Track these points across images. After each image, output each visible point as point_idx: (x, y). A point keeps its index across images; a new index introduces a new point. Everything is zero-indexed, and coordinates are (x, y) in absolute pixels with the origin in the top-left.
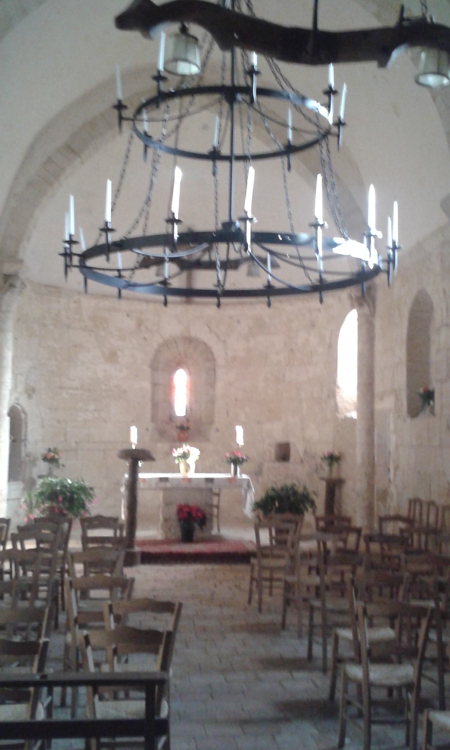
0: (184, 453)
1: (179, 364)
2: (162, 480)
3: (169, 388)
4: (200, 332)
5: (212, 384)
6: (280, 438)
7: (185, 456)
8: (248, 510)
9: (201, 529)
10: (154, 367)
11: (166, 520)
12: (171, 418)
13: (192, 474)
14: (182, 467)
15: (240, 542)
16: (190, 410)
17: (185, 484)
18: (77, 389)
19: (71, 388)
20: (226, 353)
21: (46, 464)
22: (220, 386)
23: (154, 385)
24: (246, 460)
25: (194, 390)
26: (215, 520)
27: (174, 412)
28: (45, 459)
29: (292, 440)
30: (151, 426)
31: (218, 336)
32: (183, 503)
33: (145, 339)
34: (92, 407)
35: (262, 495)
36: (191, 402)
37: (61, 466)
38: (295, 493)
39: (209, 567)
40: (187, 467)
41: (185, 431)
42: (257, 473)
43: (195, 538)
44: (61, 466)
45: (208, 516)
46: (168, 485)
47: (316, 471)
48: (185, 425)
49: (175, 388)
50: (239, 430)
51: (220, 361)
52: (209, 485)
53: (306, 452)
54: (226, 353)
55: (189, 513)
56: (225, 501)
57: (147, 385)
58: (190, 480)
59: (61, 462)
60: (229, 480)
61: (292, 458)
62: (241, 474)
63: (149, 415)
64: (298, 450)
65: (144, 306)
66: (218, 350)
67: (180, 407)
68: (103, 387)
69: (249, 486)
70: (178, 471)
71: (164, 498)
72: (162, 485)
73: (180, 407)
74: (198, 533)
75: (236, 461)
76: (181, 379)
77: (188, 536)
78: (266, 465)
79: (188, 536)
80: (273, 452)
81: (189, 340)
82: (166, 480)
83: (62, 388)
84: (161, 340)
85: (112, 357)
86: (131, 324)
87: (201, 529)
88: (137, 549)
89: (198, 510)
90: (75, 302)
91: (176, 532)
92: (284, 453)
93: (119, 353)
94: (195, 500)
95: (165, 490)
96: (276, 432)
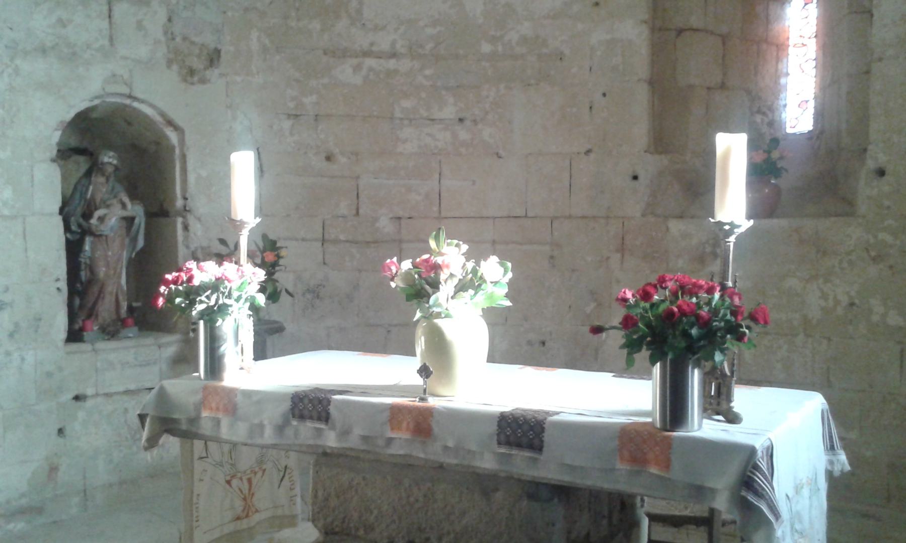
18: (394, 55)
19: (367, 54)
34: (449, 112)
50: (243, 165)
68: (486, 48)
72: (306, 430)
83: (340, 54)
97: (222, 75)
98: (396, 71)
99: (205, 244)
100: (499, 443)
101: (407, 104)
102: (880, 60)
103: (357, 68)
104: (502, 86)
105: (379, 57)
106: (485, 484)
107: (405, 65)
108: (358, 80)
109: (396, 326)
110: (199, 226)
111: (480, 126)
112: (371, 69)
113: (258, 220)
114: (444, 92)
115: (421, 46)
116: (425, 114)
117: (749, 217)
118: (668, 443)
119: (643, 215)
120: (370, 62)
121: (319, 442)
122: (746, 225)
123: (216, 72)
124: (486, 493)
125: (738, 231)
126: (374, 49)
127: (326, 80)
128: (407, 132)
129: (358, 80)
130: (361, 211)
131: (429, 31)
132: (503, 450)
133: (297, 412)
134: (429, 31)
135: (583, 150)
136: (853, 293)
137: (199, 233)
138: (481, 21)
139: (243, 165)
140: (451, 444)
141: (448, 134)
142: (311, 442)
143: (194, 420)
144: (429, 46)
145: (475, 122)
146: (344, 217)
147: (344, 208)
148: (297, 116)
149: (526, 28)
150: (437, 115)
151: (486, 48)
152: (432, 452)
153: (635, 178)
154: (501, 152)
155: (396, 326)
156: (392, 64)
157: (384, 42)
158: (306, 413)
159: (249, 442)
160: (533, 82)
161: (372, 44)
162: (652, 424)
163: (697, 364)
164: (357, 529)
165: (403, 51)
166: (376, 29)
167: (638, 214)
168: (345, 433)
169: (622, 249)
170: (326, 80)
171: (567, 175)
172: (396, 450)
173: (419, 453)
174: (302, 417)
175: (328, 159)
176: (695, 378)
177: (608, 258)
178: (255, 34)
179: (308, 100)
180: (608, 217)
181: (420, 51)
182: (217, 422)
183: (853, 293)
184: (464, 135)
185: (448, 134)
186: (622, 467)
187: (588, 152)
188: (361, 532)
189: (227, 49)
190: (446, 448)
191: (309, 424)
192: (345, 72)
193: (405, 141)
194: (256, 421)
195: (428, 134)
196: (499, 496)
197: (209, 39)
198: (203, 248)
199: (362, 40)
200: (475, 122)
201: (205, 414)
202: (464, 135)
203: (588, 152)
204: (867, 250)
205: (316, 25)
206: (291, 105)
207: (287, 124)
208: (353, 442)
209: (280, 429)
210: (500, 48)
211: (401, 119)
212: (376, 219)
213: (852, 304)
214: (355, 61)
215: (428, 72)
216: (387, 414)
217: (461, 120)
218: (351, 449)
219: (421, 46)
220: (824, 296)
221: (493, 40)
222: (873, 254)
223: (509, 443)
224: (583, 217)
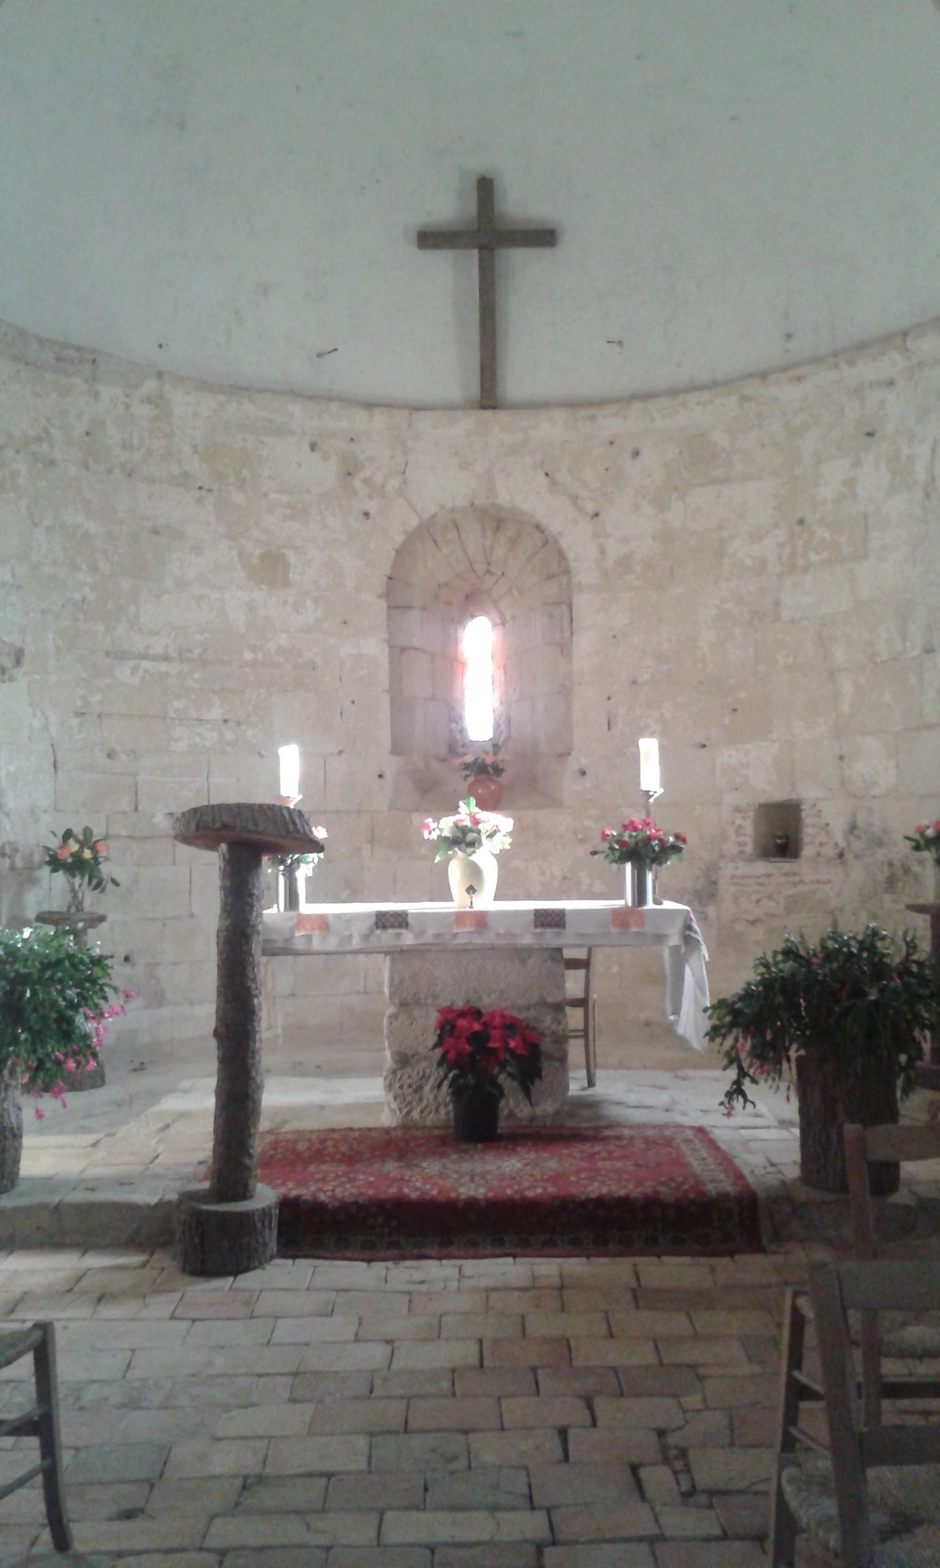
0: (464, 831)
1: (471, 601)
2: (383, 921)
3: (446, 664)
4: (524, 493)
5: (565, 648)
6: (769, 788)
7: (464, 839)
8: (691, 1020)
9: (528, 1094)
10: (396, 594)
11: (403, 1060)
12: (455, 745)
13: (486, 902)
14: (455, 873)
15: (661, 1140)
16: (505, 723)
17: (464, 935)
18: (166, 658)
19: (144, 656)
20: (603, 551)
21: (60, 876)
22: (585, 644)
23: (399, 652)
24: (675, 849)
25: (515, 665)
26: (575, 1050)
27: (462, 731)
28: (55, 863)
29: (807, 793)
30: (392, 766)
31: (574, 499)
32: (460, 1004)
33: (366, 514)
34: (215, 713)
35: (743, 976)
36: (506, 702)
37: (110, 886)
38: (879, 970)
39: (548, 1268)
40: (474, 872)
41: (490, 777)
42: (704, 894)
43: (503, 1125)
44: (110, 886)
45: (546, 1045)
46: (408, 939)
47: (891, 882)
48: (489, 760)
49: (463, 664)
50: (649, 748)
51: (585, 572)
52: (550, 937)
53: (853, 828)
54: (603, 551)
55: (479, 1040)
56: (608, 981)
57: (375, 648)
58: (481, 920)
59: (106, 869)
60: (620, 918)
61: (808, 851)
62: (657, 902)
63: (385, 737)
64: (825, 819)
65: (360, 418)
66: (577, 542)
67: (480, 716)
68: (248, 656)
69: (688, 939)
70: (447, 896)
71: (396, 986)
72: (387, 937)
73: (480, 716)
74: (514, 1107)
75: (641, 852)
76: (479, 640)
77: (477, 1124)
78: (728, 870)
79: (477, 1124)
80: (746, 832)
81: (496, 519)
82: (399, 920)
83: (118, 655)
84: (414, 522)
85: (271, 568)
86: (322, 472)
87: (528, 1094)
88: (264, 1195)
89: (511, 1026)
90: (149, 401)
91: (437, 1107)
92: (781, 834)
93: (291, 557)
94: (501, 991)
95: (398, 954)
96: (758, 771)
97: (26, 674)
98: (168, 674)
99: (12, 838)
100: (536, 926)
101: (178, 704)
102: (579, 684)
103: (134, 670)
104: (262, 691)
105: (154, 658)
106: (521, 954)
107: (174, 668)
108: (135, 681)
109: (171, 919)
110: (7, 821)
111: (243, 727)
112: (146, 671)
113: (301, 797)
114: (211, 695)
115: (190, 651)
116: (195, 715)
117: (662, 786)
118: (641, 915)
119: (389, 810)
120: (146, 664)
121: (398, 943)
122: (661, 791)
123: (22, 670)
124: (523, 961)
125: (656, 795)
126: (151, 652)
127: (108, 681)
128: (178, 732)
129: (135, 681)
130: (140, 808)
131: (198, 637)
132: (539, 930)
133: (380, 924)
134: (198, 637)
135: (336, 751)
136: (566, 870)
137: (8, 828)
138: (243, 630)
139: (649, 748)
140: (502, 931)
141: (215, 734)
142: (392, 944)
143: (289, 940)
144: (197, 651)
145: (239, 723)
146: (124, 813)
147: (125, 803)
148: (83, 714)
149: (283, 640)
150: (206, 716)
151: (248, 656)
152: (488, 938)
153: (380, 776)
154: (263, 752)
155: (171, 919)
156: (163, 667)
157: (158, 646)
158: (387, 924)
159: (340, 949)
160: (290, 688)
161: (148, 647)
162: (626, 906)
163: (651, 870)
164: (426, 999)
165: (174, 654)
166: (152, 633)
167: (385, 807)
168: (421, 933)
169: (372, 840)
170: (108, 681)
171: (322, 773)
172: (461, 940)
173: (478, 940)
174: (384, 927)
175: (109, 756)
176: (650, 877)
177: (360, 849)
178: (51, 635)
179: (95, 698)
180: (359, 812)
181: (189, 655)
182: (309, 938)
183: (566, 870)
184: (229, 735)
185: (215, 734)
186: (614, 930)
187: (340, 753)
188: (430, 1001)
189: (29, 650)
190: (498, 935)
191: (391, 931)
192: (124, 672)
193: (177, 740)
194: (347, 933)
195: (197, 734)
196: (531, 961)
197: (14, 639)
198: (10, 843)
199: (140, 645)
200: (239, 723)
201: (298, 934)
202: (229, 735)
203: (340, 753)
204: (575, 834)
205: (100, 628)
206: (79, 703)
207: (75, 722)
208: (428, 938)
209: (366, 937)
210: (260, 656)
211: (173, 719)
212: (153, 816)
213: (565, 878)
214: (133, 663)
215: (196, 676)
216: (453, 918)
217: (225, 721)
218: (426, 944)
219: (190, 651)
220: (543, 873)
221: (254, 649)
222: (580, 837)
223: (542, 925)
224: (338, 812)
